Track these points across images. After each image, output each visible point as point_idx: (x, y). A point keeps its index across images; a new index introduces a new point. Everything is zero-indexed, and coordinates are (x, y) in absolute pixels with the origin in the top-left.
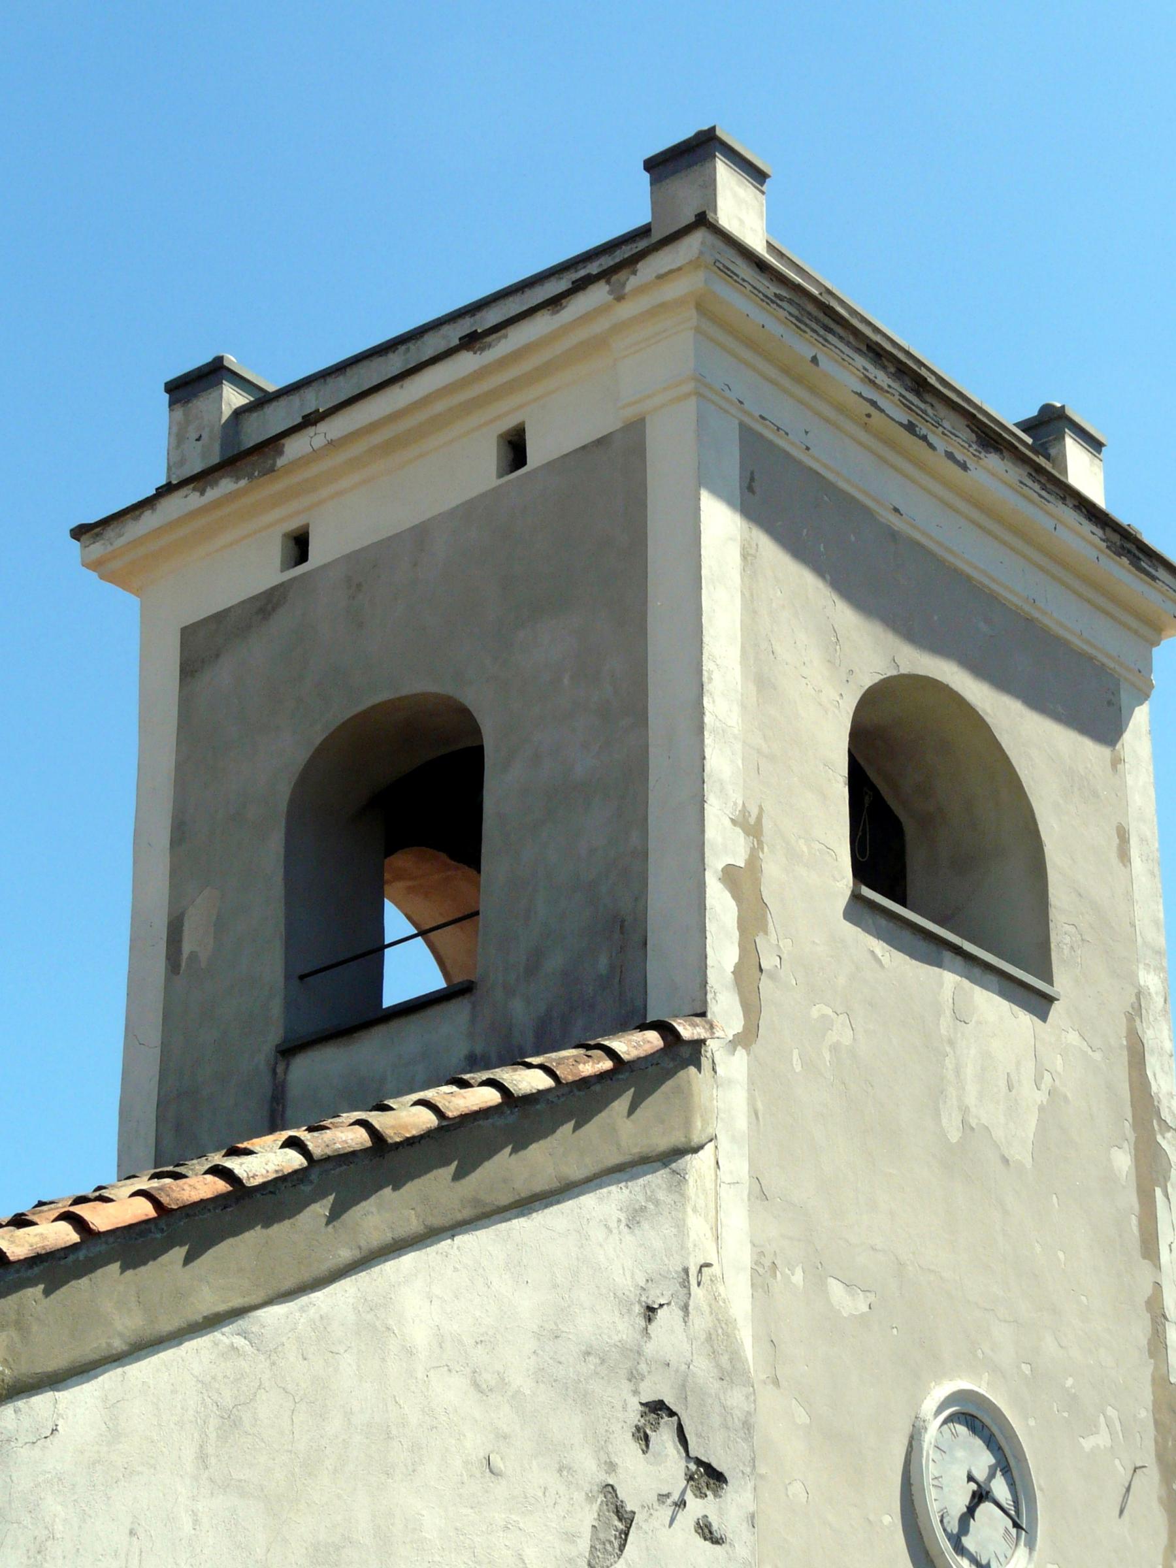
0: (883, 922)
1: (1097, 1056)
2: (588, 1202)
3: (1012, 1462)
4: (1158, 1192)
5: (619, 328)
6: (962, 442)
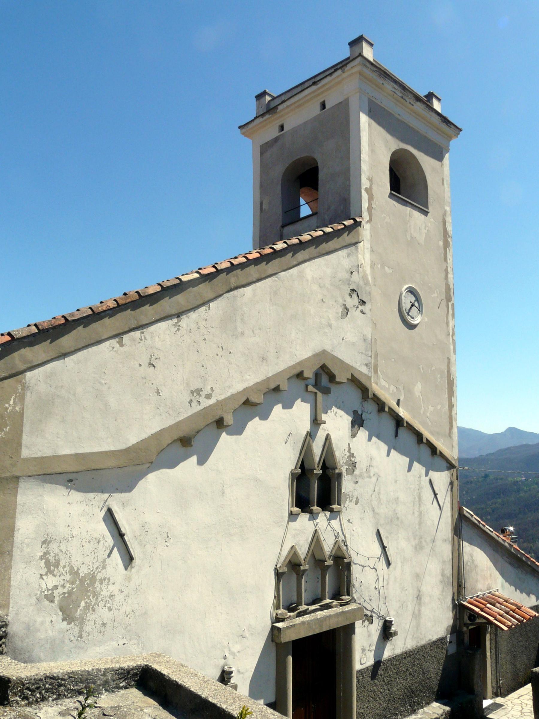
4: (448, 249)
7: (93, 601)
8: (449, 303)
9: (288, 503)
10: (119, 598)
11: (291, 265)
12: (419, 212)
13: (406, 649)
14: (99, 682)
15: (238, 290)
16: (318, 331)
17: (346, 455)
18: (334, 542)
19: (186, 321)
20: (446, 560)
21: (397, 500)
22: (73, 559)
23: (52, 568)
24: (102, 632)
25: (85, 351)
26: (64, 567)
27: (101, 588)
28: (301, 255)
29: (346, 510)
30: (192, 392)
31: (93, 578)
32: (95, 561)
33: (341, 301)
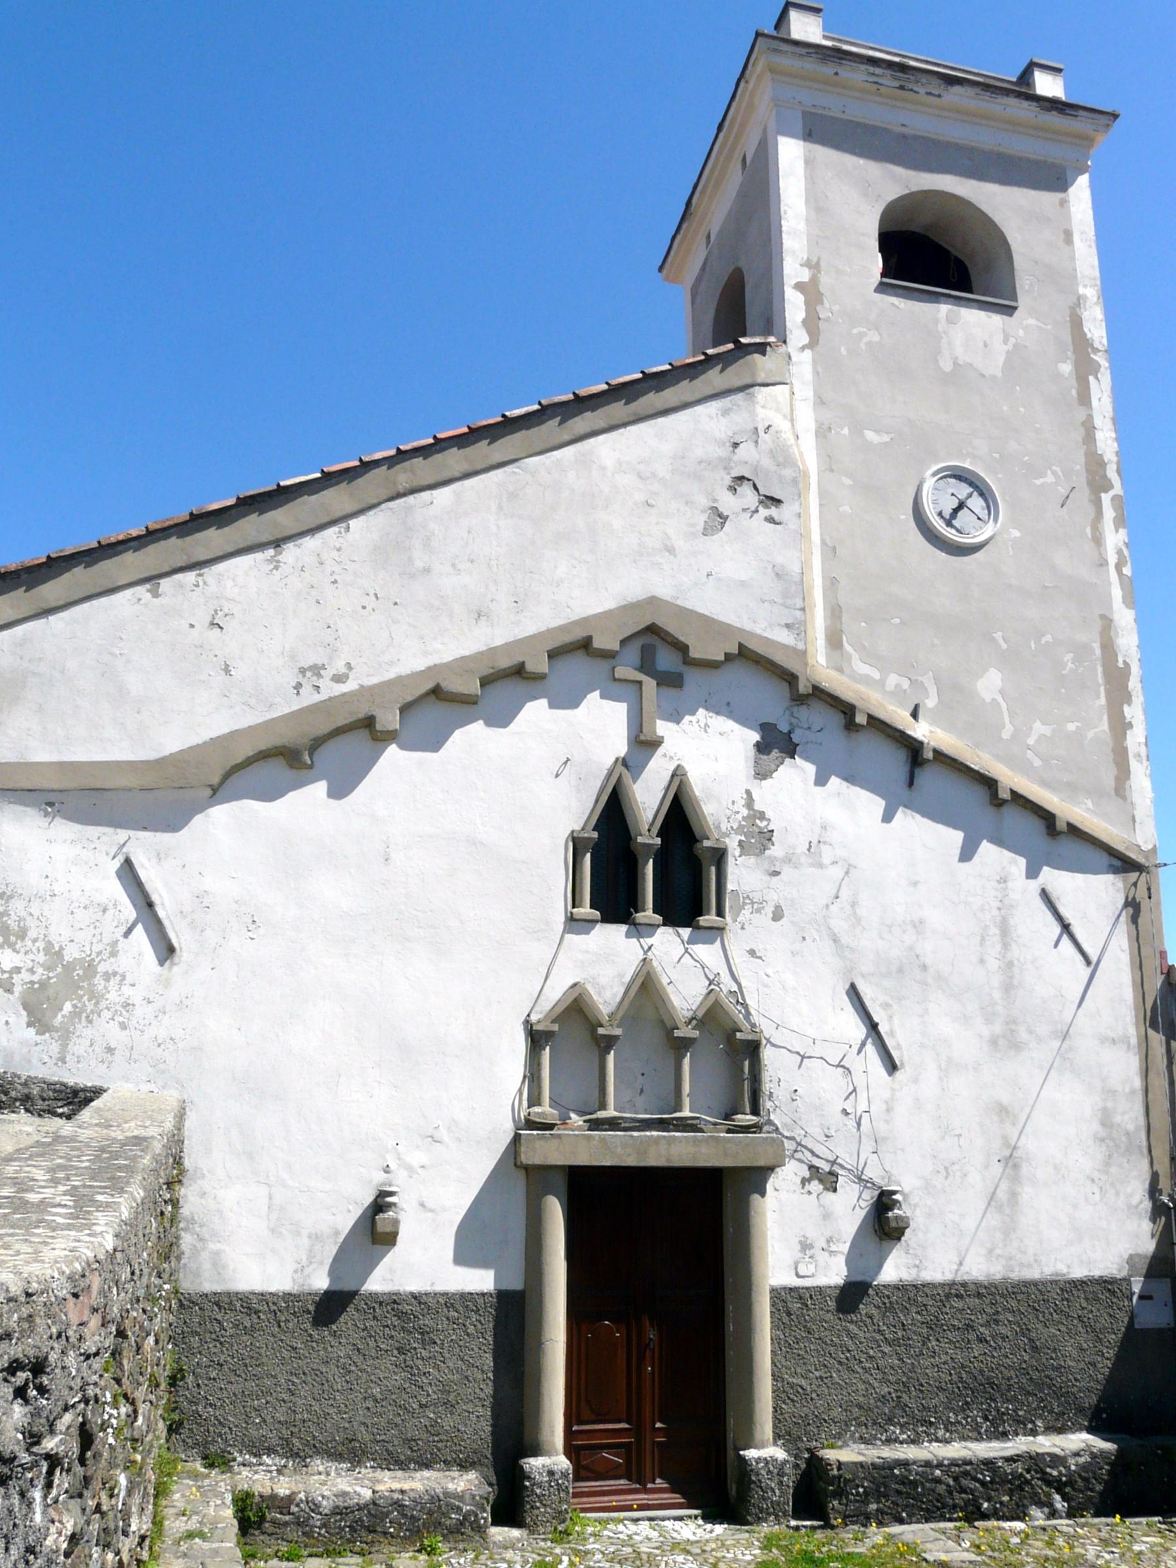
0: (900, 291)
1: (1049, 327)
2: (699, 409)
3: (984, 491)
4: (1091, 378)
5: (752, 96)
6: (936, 86)
7: (90, 1006)
8: (1103, 495)
9: (563, 898)
10: (142, 1011)
11: (557, 442)
12: (979, 309)
13: (965, 1278)
14: (13, 1094)
15: (416, 495)
16: (635, 562)
17: (738, 812)
18: (705, 992)
19: (290, 552)
20: (1120, 1089)
21: (918, 925)
22: (52, 929)
23: (13, 939)
24: (107, 1063)
25: (86, 606)
26: (35, 941)
27: (106, 988)
28: (581, 423)
29: (743, 928)
30: (303, 671)
31: (90, 969)
32: (95, 940)
33: (704, 502)
